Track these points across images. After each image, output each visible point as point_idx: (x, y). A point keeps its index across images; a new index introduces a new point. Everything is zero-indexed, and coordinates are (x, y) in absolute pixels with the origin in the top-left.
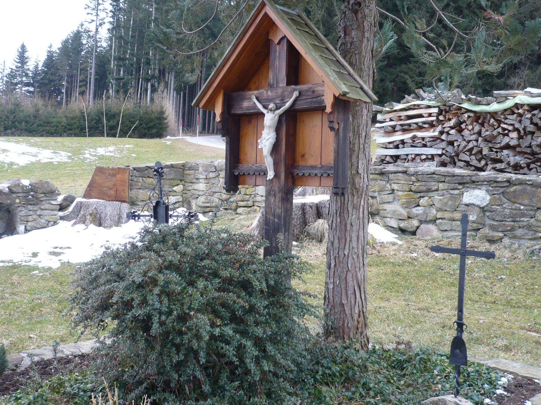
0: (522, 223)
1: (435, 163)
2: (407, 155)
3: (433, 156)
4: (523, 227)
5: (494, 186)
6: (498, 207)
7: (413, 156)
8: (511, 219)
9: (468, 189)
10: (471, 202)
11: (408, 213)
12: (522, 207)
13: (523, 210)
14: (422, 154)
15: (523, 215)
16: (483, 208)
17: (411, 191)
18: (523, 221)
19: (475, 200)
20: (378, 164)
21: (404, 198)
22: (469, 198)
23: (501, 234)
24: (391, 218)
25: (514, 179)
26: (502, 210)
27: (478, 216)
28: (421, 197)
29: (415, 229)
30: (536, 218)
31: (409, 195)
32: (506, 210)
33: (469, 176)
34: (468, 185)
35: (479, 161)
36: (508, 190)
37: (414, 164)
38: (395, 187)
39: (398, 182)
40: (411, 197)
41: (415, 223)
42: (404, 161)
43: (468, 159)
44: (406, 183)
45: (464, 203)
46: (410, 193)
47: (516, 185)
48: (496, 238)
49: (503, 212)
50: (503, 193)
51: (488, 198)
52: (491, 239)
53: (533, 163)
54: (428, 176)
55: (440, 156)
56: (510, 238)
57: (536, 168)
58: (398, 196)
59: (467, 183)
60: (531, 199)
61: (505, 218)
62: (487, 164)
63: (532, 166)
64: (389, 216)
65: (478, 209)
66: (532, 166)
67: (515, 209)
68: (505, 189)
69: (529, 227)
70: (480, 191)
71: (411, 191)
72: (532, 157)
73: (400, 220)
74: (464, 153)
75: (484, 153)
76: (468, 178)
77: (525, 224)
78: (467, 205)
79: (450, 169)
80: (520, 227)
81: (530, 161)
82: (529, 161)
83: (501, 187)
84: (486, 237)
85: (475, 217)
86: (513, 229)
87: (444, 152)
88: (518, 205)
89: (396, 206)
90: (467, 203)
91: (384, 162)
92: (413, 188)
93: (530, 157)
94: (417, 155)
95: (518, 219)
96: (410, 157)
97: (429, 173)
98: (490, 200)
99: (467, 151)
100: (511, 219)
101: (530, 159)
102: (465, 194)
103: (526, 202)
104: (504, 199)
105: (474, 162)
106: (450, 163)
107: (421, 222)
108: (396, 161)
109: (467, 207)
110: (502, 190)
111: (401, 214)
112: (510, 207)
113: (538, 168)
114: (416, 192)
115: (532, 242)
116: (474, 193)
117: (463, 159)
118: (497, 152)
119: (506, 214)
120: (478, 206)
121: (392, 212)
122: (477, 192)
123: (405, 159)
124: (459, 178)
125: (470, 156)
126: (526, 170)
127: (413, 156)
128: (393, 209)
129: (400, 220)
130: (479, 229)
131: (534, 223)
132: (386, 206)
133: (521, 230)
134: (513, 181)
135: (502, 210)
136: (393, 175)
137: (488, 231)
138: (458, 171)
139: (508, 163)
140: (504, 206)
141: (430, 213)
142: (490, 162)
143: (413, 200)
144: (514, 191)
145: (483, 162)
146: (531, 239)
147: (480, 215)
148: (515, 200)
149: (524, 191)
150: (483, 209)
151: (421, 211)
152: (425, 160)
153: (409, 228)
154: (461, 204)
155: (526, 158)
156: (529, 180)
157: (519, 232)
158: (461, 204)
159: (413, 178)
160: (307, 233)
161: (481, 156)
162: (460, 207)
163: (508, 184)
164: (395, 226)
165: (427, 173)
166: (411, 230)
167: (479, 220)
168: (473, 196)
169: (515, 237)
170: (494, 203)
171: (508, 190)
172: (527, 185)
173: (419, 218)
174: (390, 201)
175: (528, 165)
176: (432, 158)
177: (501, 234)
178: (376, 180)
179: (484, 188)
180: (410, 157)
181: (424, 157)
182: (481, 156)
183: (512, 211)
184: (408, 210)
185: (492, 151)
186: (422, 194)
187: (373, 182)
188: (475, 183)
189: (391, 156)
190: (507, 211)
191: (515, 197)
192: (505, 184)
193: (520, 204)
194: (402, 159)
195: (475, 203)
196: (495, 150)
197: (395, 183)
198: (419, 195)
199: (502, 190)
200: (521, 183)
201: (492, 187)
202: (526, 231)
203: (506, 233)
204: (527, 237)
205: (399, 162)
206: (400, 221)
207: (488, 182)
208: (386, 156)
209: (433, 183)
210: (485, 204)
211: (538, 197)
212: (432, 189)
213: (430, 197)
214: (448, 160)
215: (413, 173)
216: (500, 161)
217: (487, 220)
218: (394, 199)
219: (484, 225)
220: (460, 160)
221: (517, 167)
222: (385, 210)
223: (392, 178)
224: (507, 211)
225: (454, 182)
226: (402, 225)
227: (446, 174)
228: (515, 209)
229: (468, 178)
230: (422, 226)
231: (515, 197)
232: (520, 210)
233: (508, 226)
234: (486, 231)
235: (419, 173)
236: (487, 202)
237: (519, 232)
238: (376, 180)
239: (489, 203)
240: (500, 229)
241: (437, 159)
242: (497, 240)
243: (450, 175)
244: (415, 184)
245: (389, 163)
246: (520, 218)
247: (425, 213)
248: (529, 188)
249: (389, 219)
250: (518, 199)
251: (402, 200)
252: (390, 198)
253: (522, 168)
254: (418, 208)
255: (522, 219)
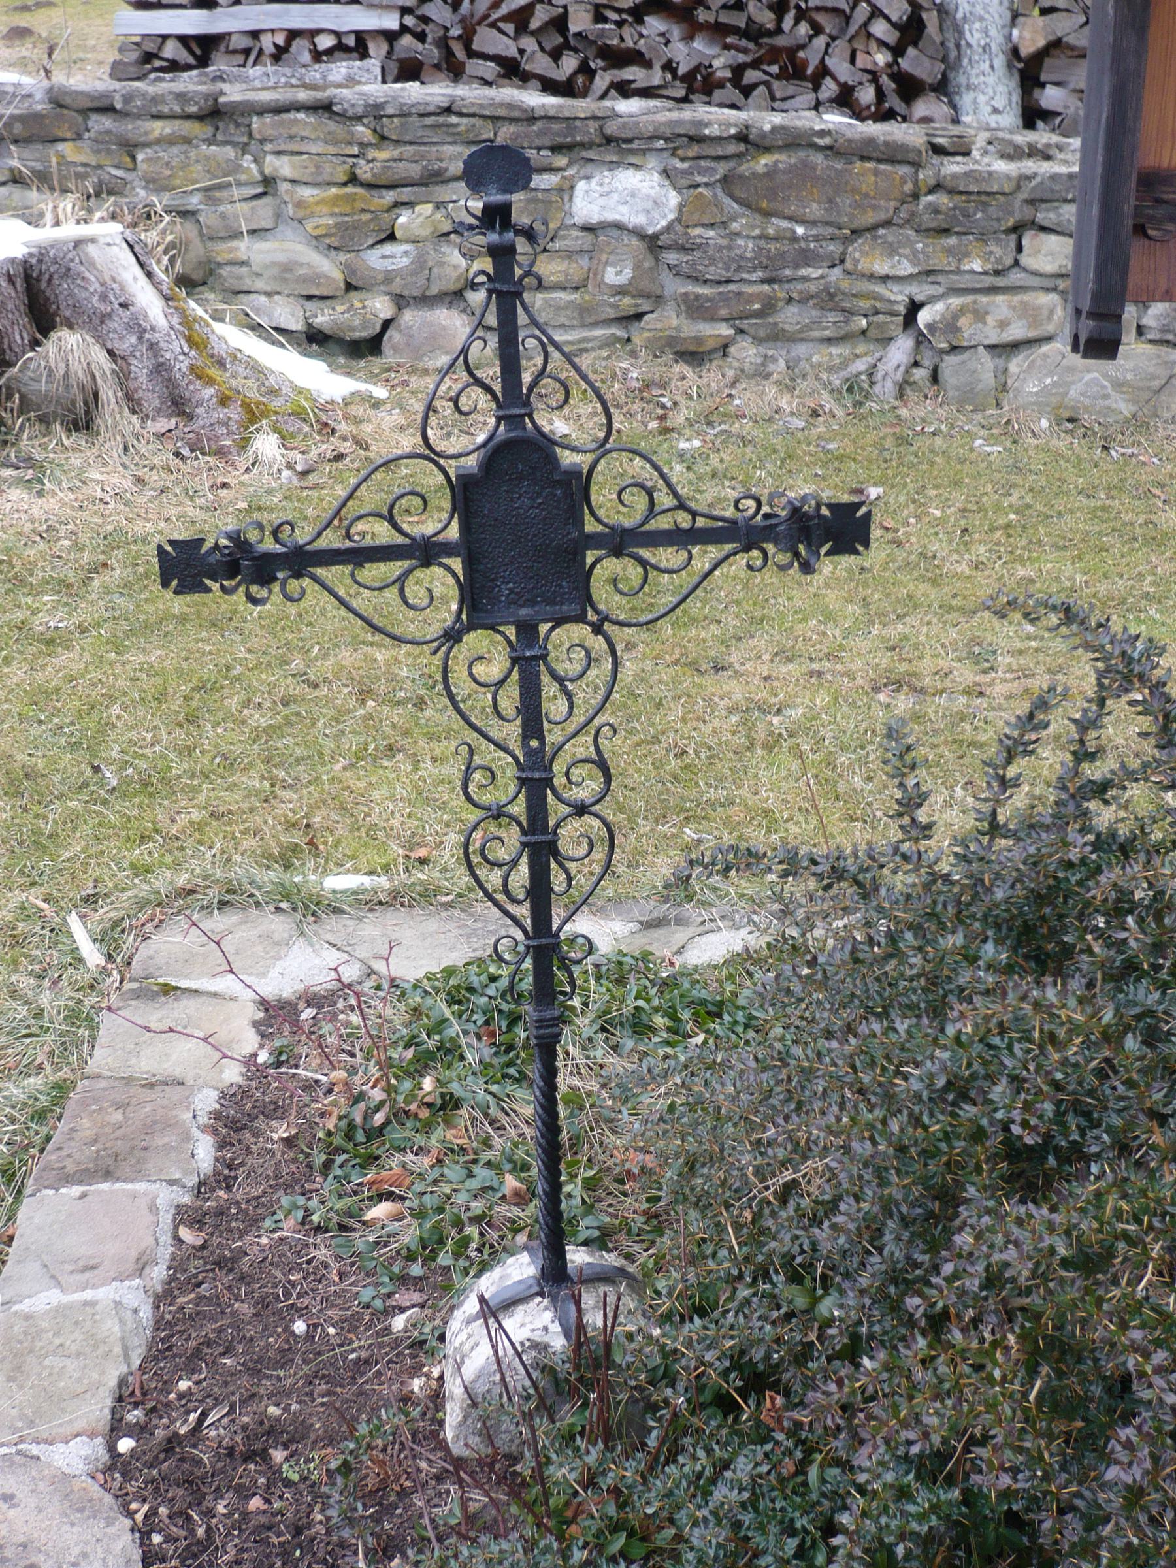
0: (800, 286)
1: (374, 64)
2: (255, 34)
3: (361, 37)
4: (804, 300)
5: (690, 154)
6: (711, 233)
7: (280, 40)
8: (760, 274)
9: (589, 169)
10: (611, 216)
11: (348, 268)
12: (800, 230)
13: (805, 238)
14: (318, 32)
15: (807, 258)
16: (655, 237)
17: (353, 179)
18: (805, 279)
19: (624, 209)
20: (133, 71)
21: (325, 209)
22: (602, 201)
23: (726, 330)
24: (269, 294)
25: (767, 127)
26: (724, 242)
27: (637, 267)
28: (397, 205)
29: (378, 329)
30: (848, 265)
31: (351, 198)
32: (741, 242)
33: (595, 118)
34: (590, 154)
35: (556, 55)
36: (745, 168)
37: (288, 71)
38: (284, 167)
39: (296, 148)
40: (359, 205)
41: (382, 307)
42: (240, 58)
43: (511, 51)
44: (332, 149)
45: (578, 220)
46: (350, 189)
47: (768, 149)
48: (710, 344)
49: (730, 248)
50: (725, 181)
51: (673, 199)
52: (692, 348)
53: (755, 64)
54: (429, 121)
55: (390, 36)
56: (758, 341)
57: (767, 84)
58: (300, 204)
59: (582, 145)
60: (830, 201)
61: (739, 269)
62: (585, 69)
63: (751, 76)
64: (260, 285)
65: (635, 241)
66: (751, 76)
67: (776, 239)
68: (732, 164)
69: (828, 299)
70: (639, 175)
71: (353, 179)
72: (751, 46)
73: (310, 298)
74: (493, 25)
75: (573, 28)
76: (592, 126)
77: (813, 288)
78: (588, 229)
79: (433, 92)
80: (790, 300)
81: (747, 59)
82: (742, 58)
83: (718, 158)
84: (671, 341)
85: (628, 273)
86: (769, 307)
87: (409, 21)
88: (785, 224)
89: (288, 245)
90: (595, 219)
91: (158, 63)
92: (365, 171)
93: (744, 43)
94: (293, 34)
95: (788, 272)
96: (267, 42)
97: (431, 109)
98: (681, 207)
99: (504, 19)
100: (760, 274)
101: (745, 51)
102: (581, 186)
103: (814, 210)
104: (727, 200)
105: (541, 64)
106: (437, 67)
107: (401, 301)
108: (203, 62)
109: (589, 237)
110: (722, 169)
111: (319, 276)
112: (757, 232)
113: (776, 84)
114: (370, 186)
115: (835, 350)
116: (616, 184)
117: (491, 51)
118: (620, 24)
119: (742, 257)
120: (638, 233)
121: (275, 271)
122: (628, 179)
123: (247, 52)
124: (556, 127)
125: (515, 39)
126: (730, 93)
127: (280, 40)
128: (281, 257)
129: (310, 298)
130: (639, 316)
131: (845, 285)
132: (244, 248)
133: (793, 309)
134: (763, 135)
135: (724, 242)
136: (268, 119)
137: (675, 322)
138: (468, 93)
139: (669, 67)
140: (735, 226)
141: (441, 264)
142: (600, 63)
143: (365, 217)
144: (771, 173)
145: (569, 63)
146: (829, 340)
147: (647, 265)
148: (775, 205)
149: (804, 171)
150: (653, 243)
151: (405, 261)
152: (329, 52)
153: (353, 329)
154: (568, 227)
155: (727, 47)
156: (823, 133)
157: (790, 317)
158: (568, 227)
159: (362, 131)
160: (23, 397)
161: (560, 40)
162: (564, 238)
163: (742, 147)
164: (296, 325)
165: (421, 109)
166: (359, 334)
167: (646, 285)
168: (615, 196)
169: (777, 336)
170: (696, 217)
171: (745, 168)
172: (811, 152)
173: (396, 287)
174: (263, 224)
175: (738, 71)
176: (357, 46)
177: (726, 330)
178: (188, 141)
179: (653, 162)
180: (267, 42)
181: (325, 42)
182: (560, 40)
183: (762, 243)
184: (343, 257)
185: (605, 20)
186: (405, 193)
187: (175, 150)
188: (618, 146)
189: (184, 40)
190: (746, 246)
191: (772, 194)
192: (732, 148)
193: (791, 218)
194: (235, 52)
195: (625, 220)
196: (614, 16)
197: (279, 153)
198: (390, 197)
199: (722, 169)
200: (794, 141)
201: (683, 160)
202: (814, 313)
203: (744, 324)
204: (816, 334)
205: (220, 64)
206: (309, 305)
207: (666, 140)
208: (165, 37)
209: (449, 150)
210: (664, 223)
211: (854, 191)
212: (449, 174)
213: (439, 206)
214: (429, 52)
215: (360, 110)
216: (636, 58)
217: (667, 278)
218: (278, 216)
219: (659, 299)
220: (472, 54)
221: (699, 84)
222: (243, 263)
223: (270, 132)
224: (746, 246)
225: (538, 142)
226: (323, 319)
227: (502, 112)
228: (776, 239)
229: (592, 126)
230: (409, 317)
231: (772, 194)
232: (795, 239)
233: (751, 299)
234: (668, 320)
235: (390, 110)
236: (671, 216)
237: (790, 317)
238: (188, 141)
239: (678, 220)
240: (723, 312)
241: (378, 49)
242: (711, 352)
243: (517, 114)
244: (372, 153)
245: (174, 66)
246: (797, 267)
247: (420, 263)
248: (818, 159)
249: (263, 298)
250: (786, 199)
251: (315, 221)
252: (264, 211)
253: (721, 85)
254: (388, 248)
255: (804, 272)
